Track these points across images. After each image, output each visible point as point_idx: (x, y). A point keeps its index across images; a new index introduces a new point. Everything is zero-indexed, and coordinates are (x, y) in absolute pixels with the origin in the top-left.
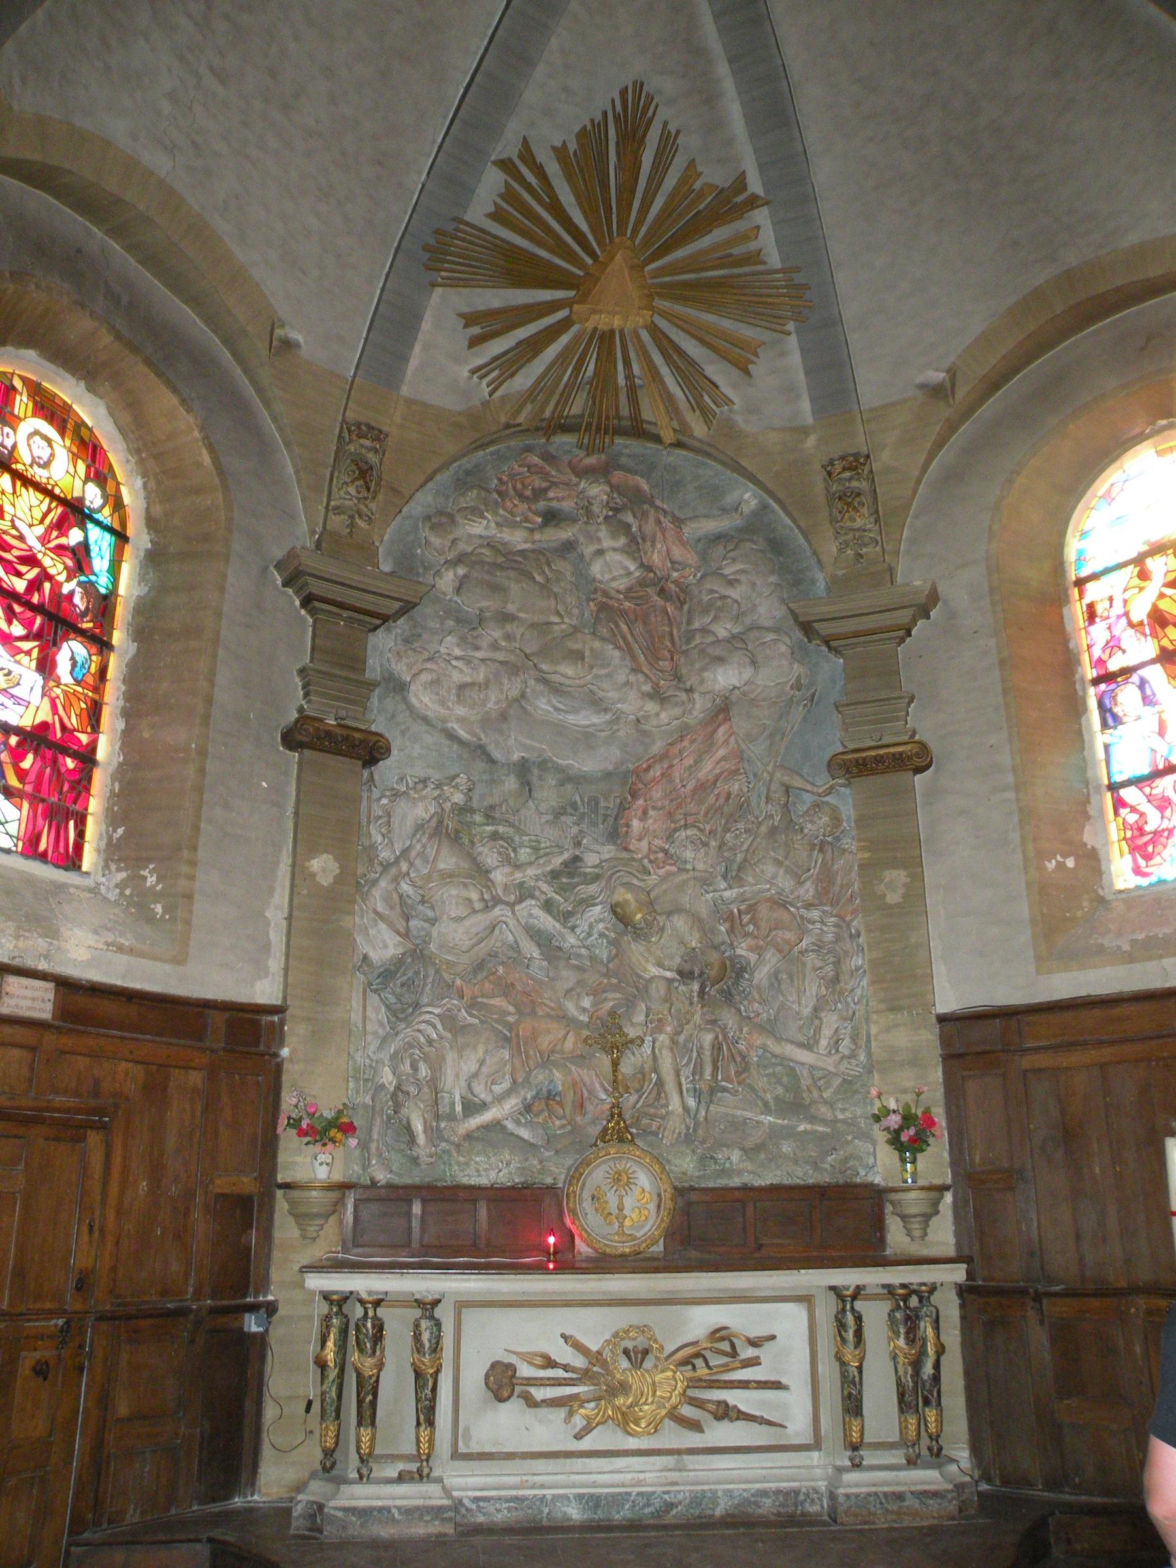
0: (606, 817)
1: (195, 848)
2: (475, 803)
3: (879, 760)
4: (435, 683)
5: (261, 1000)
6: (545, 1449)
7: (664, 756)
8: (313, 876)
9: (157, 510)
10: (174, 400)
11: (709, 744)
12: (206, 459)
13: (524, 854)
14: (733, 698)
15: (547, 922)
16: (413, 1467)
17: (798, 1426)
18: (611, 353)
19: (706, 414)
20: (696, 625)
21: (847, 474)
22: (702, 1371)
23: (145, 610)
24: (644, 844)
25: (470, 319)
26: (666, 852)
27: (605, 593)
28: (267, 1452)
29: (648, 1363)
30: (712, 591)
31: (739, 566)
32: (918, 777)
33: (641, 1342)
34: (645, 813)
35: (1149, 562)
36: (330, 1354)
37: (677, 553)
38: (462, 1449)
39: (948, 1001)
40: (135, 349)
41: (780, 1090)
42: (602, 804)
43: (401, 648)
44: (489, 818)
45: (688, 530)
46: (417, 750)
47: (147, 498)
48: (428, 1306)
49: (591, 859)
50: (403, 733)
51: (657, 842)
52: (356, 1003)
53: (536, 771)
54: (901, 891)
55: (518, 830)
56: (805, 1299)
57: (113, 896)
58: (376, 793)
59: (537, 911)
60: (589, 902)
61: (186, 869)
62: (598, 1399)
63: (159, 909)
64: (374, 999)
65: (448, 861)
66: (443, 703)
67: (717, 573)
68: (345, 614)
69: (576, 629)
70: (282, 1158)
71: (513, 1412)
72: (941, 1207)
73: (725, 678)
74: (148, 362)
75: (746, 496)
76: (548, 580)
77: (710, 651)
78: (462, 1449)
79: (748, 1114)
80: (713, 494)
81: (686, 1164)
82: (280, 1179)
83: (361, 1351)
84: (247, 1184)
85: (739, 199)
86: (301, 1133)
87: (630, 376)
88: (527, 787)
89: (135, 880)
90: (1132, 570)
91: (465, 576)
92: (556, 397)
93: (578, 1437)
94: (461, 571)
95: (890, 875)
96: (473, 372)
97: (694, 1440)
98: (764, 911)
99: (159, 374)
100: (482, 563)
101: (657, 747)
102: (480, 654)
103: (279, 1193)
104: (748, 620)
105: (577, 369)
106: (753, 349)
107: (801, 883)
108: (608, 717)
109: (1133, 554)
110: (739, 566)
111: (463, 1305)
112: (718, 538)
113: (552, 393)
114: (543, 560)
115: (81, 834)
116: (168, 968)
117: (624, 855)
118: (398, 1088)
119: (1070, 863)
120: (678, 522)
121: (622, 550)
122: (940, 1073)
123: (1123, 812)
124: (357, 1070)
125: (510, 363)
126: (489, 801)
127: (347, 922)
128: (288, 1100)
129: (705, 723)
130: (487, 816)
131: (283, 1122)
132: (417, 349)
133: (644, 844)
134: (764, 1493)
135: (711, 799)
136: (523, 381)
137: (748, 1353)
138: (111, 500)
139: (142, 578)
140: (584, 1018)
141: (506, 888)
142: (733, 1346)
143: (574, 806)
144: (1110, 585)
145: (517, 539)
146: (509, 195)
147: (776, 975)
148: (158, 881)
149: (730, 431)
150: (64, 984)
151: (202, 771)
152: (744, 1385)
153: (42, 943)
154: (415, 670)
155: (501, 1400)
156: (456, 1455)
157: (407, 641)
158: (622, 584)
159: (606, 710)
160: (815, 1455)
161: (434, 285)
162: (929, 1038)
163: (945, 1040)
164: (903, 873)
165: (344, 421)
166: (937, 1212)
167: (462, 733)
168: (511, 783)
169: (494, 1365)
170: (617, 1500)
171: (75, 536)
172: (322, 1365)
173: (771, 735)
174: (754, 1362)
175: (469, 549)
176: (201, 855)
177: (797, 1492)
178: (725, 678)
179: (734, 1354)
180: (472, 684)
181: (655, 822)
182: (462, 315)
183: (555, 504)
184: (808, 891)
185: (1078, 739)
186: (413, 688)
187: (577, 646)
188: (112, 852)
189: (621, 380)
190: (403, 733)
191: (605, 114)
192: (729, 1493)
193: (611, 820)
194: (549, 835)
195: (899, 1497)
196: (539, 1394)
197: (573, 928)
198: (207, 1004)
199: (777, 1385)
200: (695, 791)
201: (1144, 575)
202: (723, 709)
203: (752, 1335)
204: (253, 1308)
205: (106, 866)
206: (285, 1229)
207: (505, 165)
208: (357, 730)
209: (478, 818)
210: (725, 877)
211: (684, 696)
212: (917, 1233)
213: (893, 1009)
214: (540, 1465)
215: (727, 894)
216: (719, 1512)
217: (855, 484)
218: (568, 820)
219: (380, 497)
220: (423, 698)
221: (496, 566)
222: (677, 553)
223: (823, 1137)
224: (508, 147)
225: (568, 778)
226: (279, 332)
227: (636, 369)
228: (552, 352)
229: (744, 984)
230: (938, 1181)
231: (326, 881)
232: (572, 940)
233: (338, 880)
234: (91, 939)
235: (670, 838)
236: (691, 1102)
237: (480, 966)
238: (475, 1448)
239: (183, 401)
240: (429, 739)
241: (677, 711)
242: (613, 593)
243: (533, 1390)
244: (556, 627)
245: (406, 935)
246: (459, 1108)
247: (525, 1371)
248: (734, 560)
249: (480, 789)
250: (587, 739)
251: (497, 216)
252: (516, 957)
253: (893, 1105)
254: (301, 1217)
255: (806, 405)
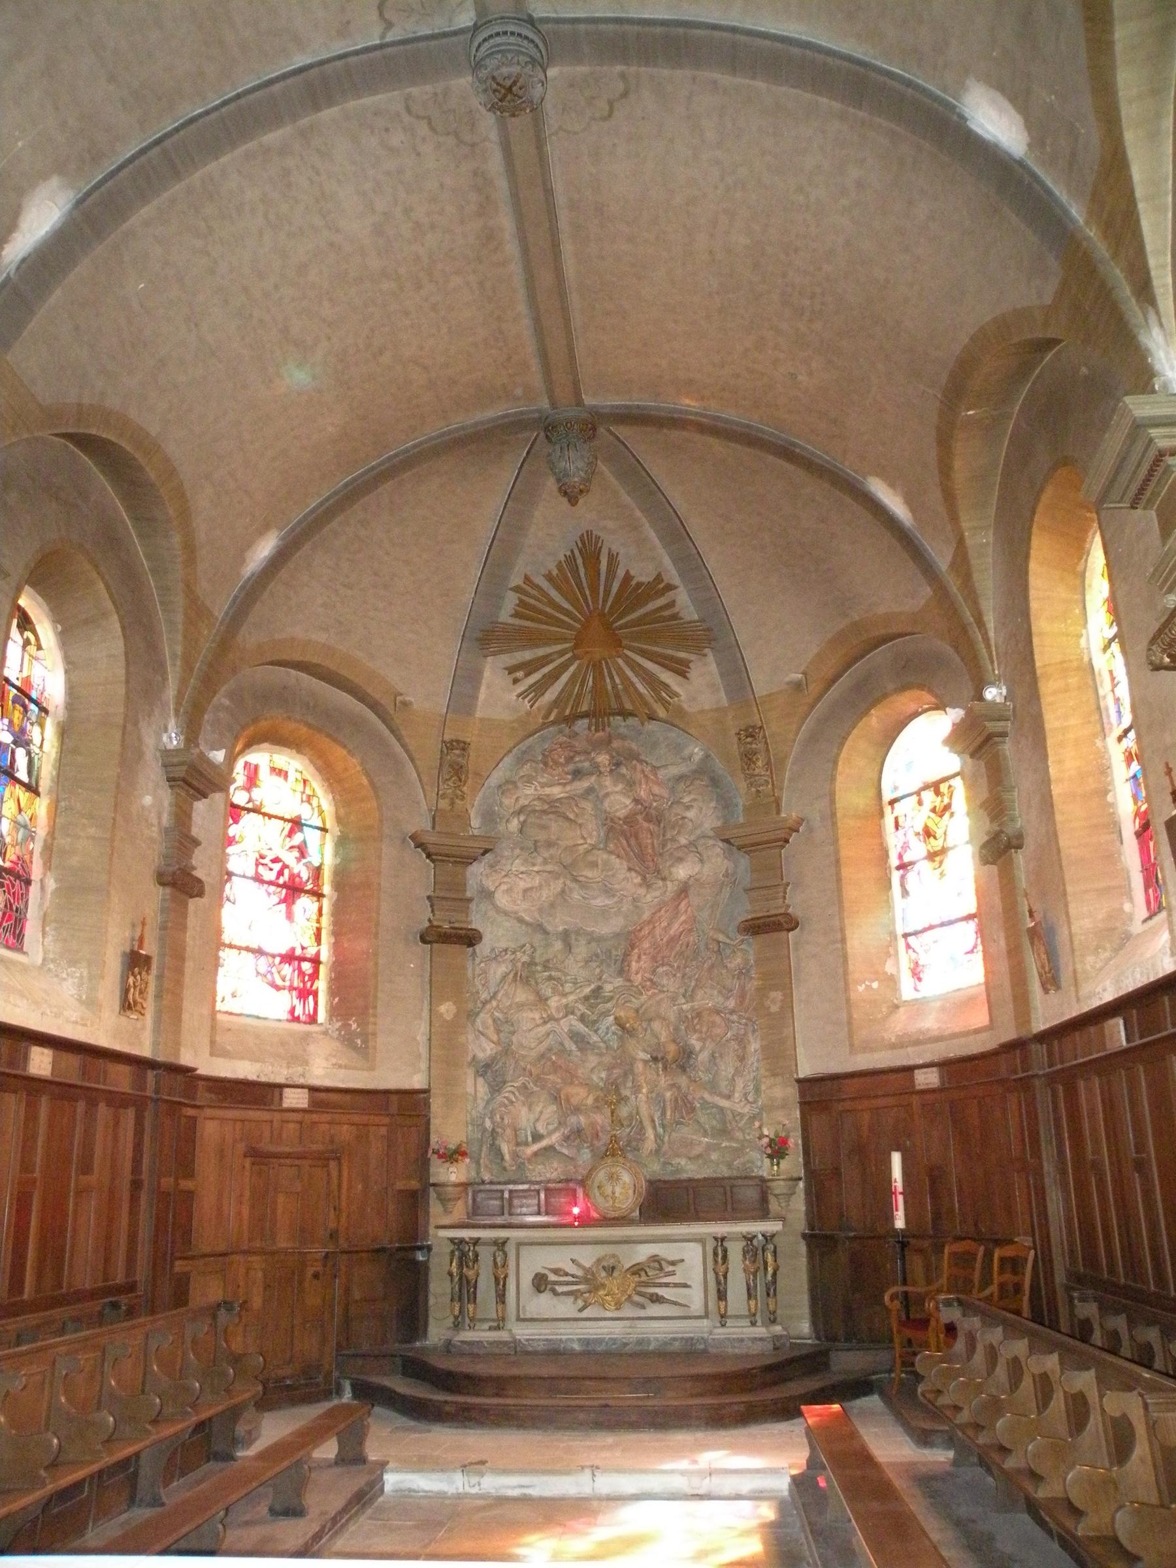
0: (616, 961)
1: (375, 1007)
2: (537, 960)
3: (765, 925)
4: (509, 891)
5: (417, 1086)
6: (562, 1316)
7: (649, 922)
8: (441, 1015)
9: (342, 812)
10: (345, 752)
11: (676, 914)
12: (365, 781)
13: (568, 987)
14: (690, 882)
15: (581, 1028)
16: (495, 1324)
17: (697, 1306)
18: (601, 673)
19: (665, 704)
20: (668, 836)
21: (749, 740)
22: (644, 1278)
23: (340, 875)
24: (639, 976)
25: (511, 670)
26: (651, 980)
27: (612, 820)
28: (431, 1320)
29: (616, 1274)
30: (677, 814)
31: (692, 796)
32: (791, 934)
33: (612, 1262)
34: (639, 957)
35: (923, 794)
36: (455, 1270)
37: (656, 790)
38: (522, 1316)
39: (806, 1069)
40: (320, 730)
41: (714, 1123)
42: (614, 953)
43: (488, 871)
44: (546, 967)
45: (662, 773)
46: (501, 932)
47: (336, 805)
48: (501, 1244)
49: (608, 987)
50: (492, 923)
51: (647, 975)
52: (470, 1080)
53: (573, 937)
54: (779, 1004)
55: (566, 974)
56: (701, 1240)
57: (336, 1034)
58: (478, 960)
59: (575, 1023)
60: (606, 1014)
61: (372, 1019)
62: (590, 1292)
63: (359, 1042)
64: (480, 1080)
65: (522, 995)
66: (514, 902)
67: (678, 802)
68: (452, 859)
69: (594, 847)
70: (432, 1170)
71: (545, 1298)
72: (797, 1190)
73: (682, 872)
74: (329, 736)
75: (696, 750)
76: (577, 815)
77: (676, 854)
78: (522, 1316)
79: (694, 1137)
80: (678, 748)
81: (655, 1168)
82: (431, 1181)
83: (468, 1267)
84: (414, 1184)
85: (661, 586)
86: (440, 1157)
87: (614, 686)
88: (568, 947)
89: (346, 1026)
90: (915, 798)
91: (525, 821)
92: (571, 702)
93: (580, 1310)
94: (522, 818)
95: (773, 994)
96: (518, 696)
97: (642, 1313)
98: (705, 1014)
99: (335, 740)
100: (535, 811)
101: (646, 916)
102: (536, 869)
103: (431, 1189)
104: (698, 832)
105: (582, 685)
106: (686, 663)
107: (728, 998)
108: (616, 899)
109: (915, 789)
110: (692, 796)
111: (520, 1244)
112: (681, 778)
113: (568, 700)
114: (573, 803)
115: (316, 1004)
116: (365, 1073)
117: (628, 984)
118: (493, 1130)
119: (875, 985)
120: (655, 769)
121: (621, 792)
122: (798, 1113)
123: (910, 951)
124: (473, 1120)
125: (539, 688)
126: (545, 957)
127: (462, 1039)
128: (434, 1139)
129: (673, 899)
130: (545, 967)
131: (430, 1152)
132: (483, 689)
133: (639, 976)
134: (675, 1339)
135: (678, 948)
136: (550, 695)
137: (671, 1268)
138: (316, 810)
139: (336, 854)
140: (601, 1084)
141: (558, 1009)
142: (660, 1265)
143: (597, 955)
144: (909, 803)
145: (556, 791)
146: (522, 603)
147: (713, 1055)
148: (358, 1026)
149: (680, 712)
150: (313, 1089)
151: (376, 964)
152: (667, 1285)
153: (300, 1069)
154: (497, 884)
155: (540, 1292)
156: (519, 1319)
157: (491, 866)
158: (622, 813)
159: (614, 896)
160: (705, 1320)
161: (486, 656)
162: (792, 1093)
163: (802, 1093)
164: (780, 993)
165: (443, 741)
166: (794, 1193)
167: (527, 918)
168: (558, 945)
169: (537, 1275)
170: (599, 1341)
171: (298, 839)
172: (450, 1274)
173: (712, 907)
174: (673, 1273)
175: (526, 803)
176: (379, 1010)
177: (692, 1339)
178: (682, 872)
179: (661, 1269)
180: (531, 888)
181: (645, 963)
182: (506, 669)
183: (580, 765)
184: (731, 1003)
185: (888, 904)
186: (496, 895)
187: (594, 859)
188: (333, 1012)
189: (609, 687)
190: (492, 923)
191: (572, 551)
192: (657, 1339)
193: (619, 963)
194: (582, 974)
195: (742, 1340)
196: (560, 1289)
197: (596, 1031)
198: (387, 1092)
199: (686, 1286)
200: (668, 942)
201: (920, 803)
202: (684, 890)
203: (671, 1258)
204: (420, 1248)
205: (331, 1019)
206: (435, 1208)
207: (517, 589)
208: (461, 929)
209: (539, 968)
210: (684, 996)
211: (660, 883)
212: (783, 1205)
213: (774, 1075)
214: (562, 1324)
215: (684, 1007)
216: (651, 1348)
217: (754, 746)
218: (594, 965)
219: (470, 781)
220: (502, 900)
221: (544, 812)
222: (656, 790)
223: (736, 1150)
224: (516, 580)
225: (593, 939)
226: (399, 698)
227: (618, 681)
228: (565, 678)
229: (692, 1062)
230: (795, 1175)
231: (448, 1017)
232: (595, 1038)
233: (456, 1015)
234: (325, 1064)
235: (654, 972)
236: (660, 1130)
237: (542, 1056)
238: (528, 1316)
239: (349, 752)
240: (508, 924)
241: (657, 893)
242: (616, 820)
243: (557, 1287)
244: (581, 848)
245: (498, 1043)
246: (530, 1139)
247: (552, 1277)
248: (690, 793)
249: (538, 952)
250: (604, 912)
251: (516, 615)
252: (563, 1051)
253: (766, 1132)
254: (443, 1200)
255: (723, 694)
